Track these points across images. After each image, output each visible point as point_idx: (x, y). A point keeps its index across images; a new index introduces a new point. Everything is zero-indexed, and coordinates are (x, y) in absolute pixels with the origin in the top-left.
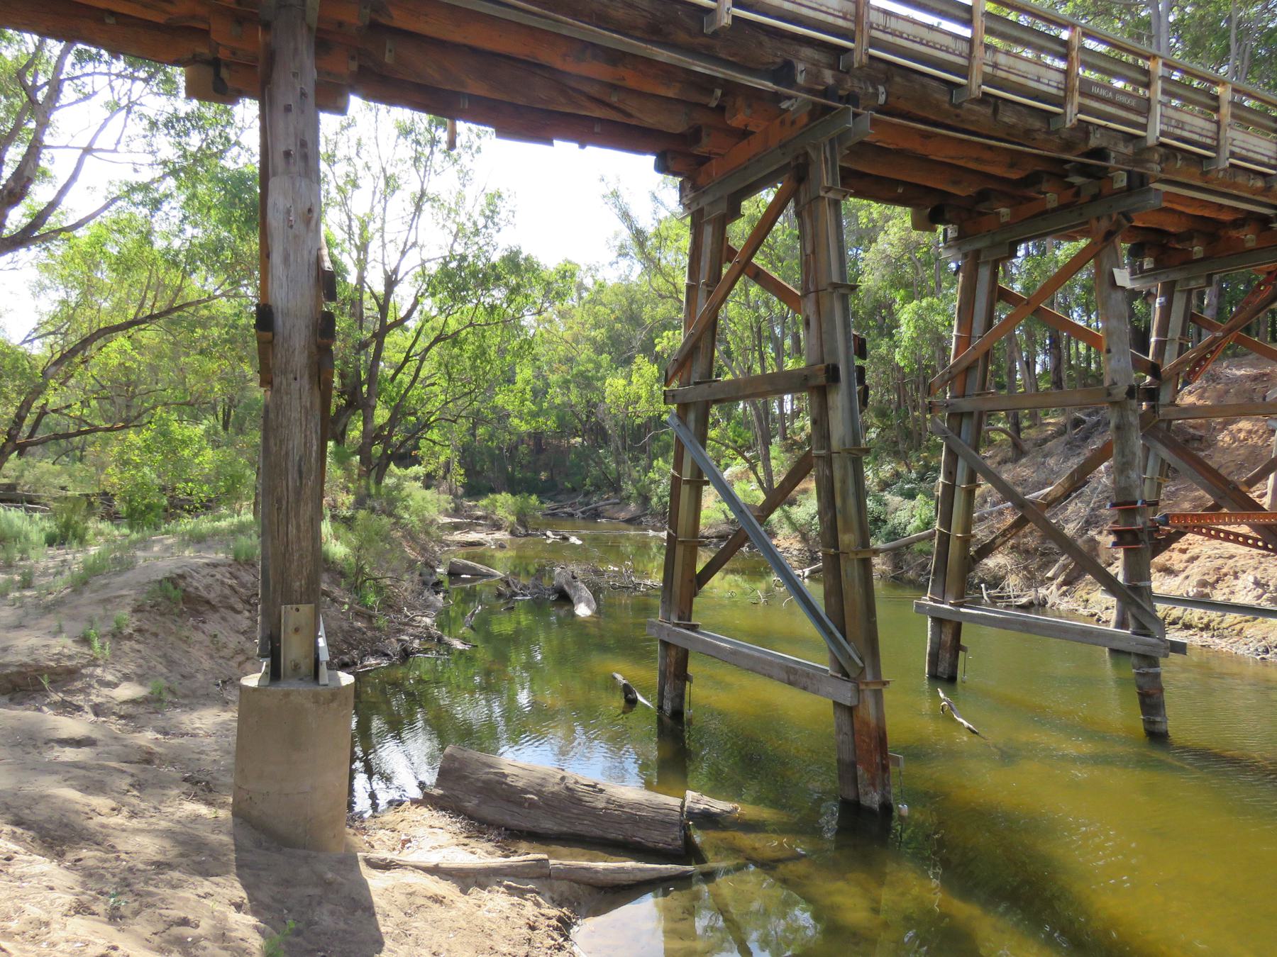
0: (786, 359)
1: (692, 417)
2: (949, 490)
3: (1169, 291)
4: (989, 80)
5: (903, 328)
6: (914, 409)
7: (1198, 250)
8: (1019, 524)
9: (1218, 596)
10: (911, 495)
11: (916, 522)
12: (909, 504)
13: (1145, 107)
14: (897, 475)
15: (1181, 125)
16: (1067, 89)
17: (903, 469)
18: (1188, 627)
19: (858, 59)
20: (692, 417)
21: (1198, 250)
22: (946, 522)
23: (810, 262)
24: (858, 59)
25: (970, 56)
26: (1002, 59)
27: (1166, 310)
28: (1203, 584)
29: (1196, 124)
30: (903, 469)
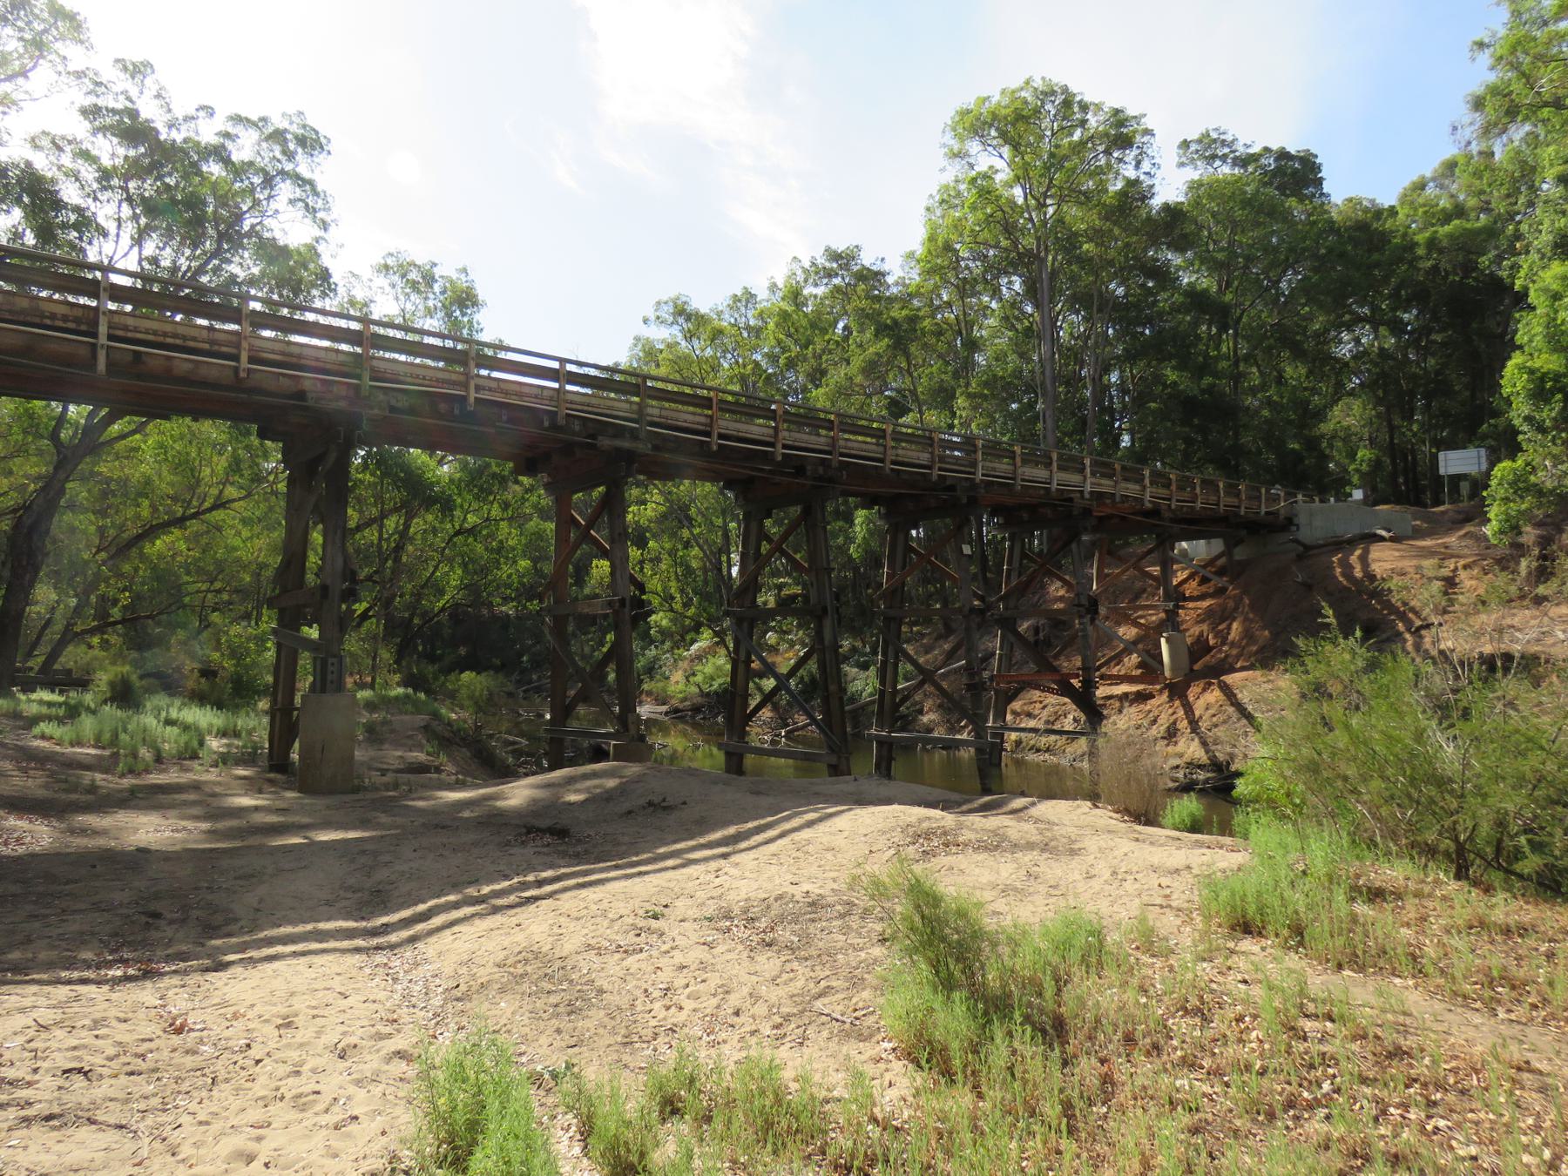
0: (850, 670)
1: (745, 625)
2: (884, 663)
3: (1012, 539)
4: (894, 463)
5: (858, 529)
6: (868, 587)
7: (1025, 516)
8: (922, 683)
9: (1057, 727)
10: (864, 667)
11: (869, 690)
12: (863, 674)
13: (974, 464)
14: (854, 650)
15: (994, 469)
16: (933, 461)
17: (859, 644)
18: (1038, 750)
19: (835, 464)
20: (745, 625)
21: (1025, 516)
22: (883, 683)
23: (812, 557)
24: (835, 464)
25: (885, 453)
26: (900, 452)
27: (1011, 548)
28: (1047, 722)
29: (1003, 466)
30: (859, 644)
